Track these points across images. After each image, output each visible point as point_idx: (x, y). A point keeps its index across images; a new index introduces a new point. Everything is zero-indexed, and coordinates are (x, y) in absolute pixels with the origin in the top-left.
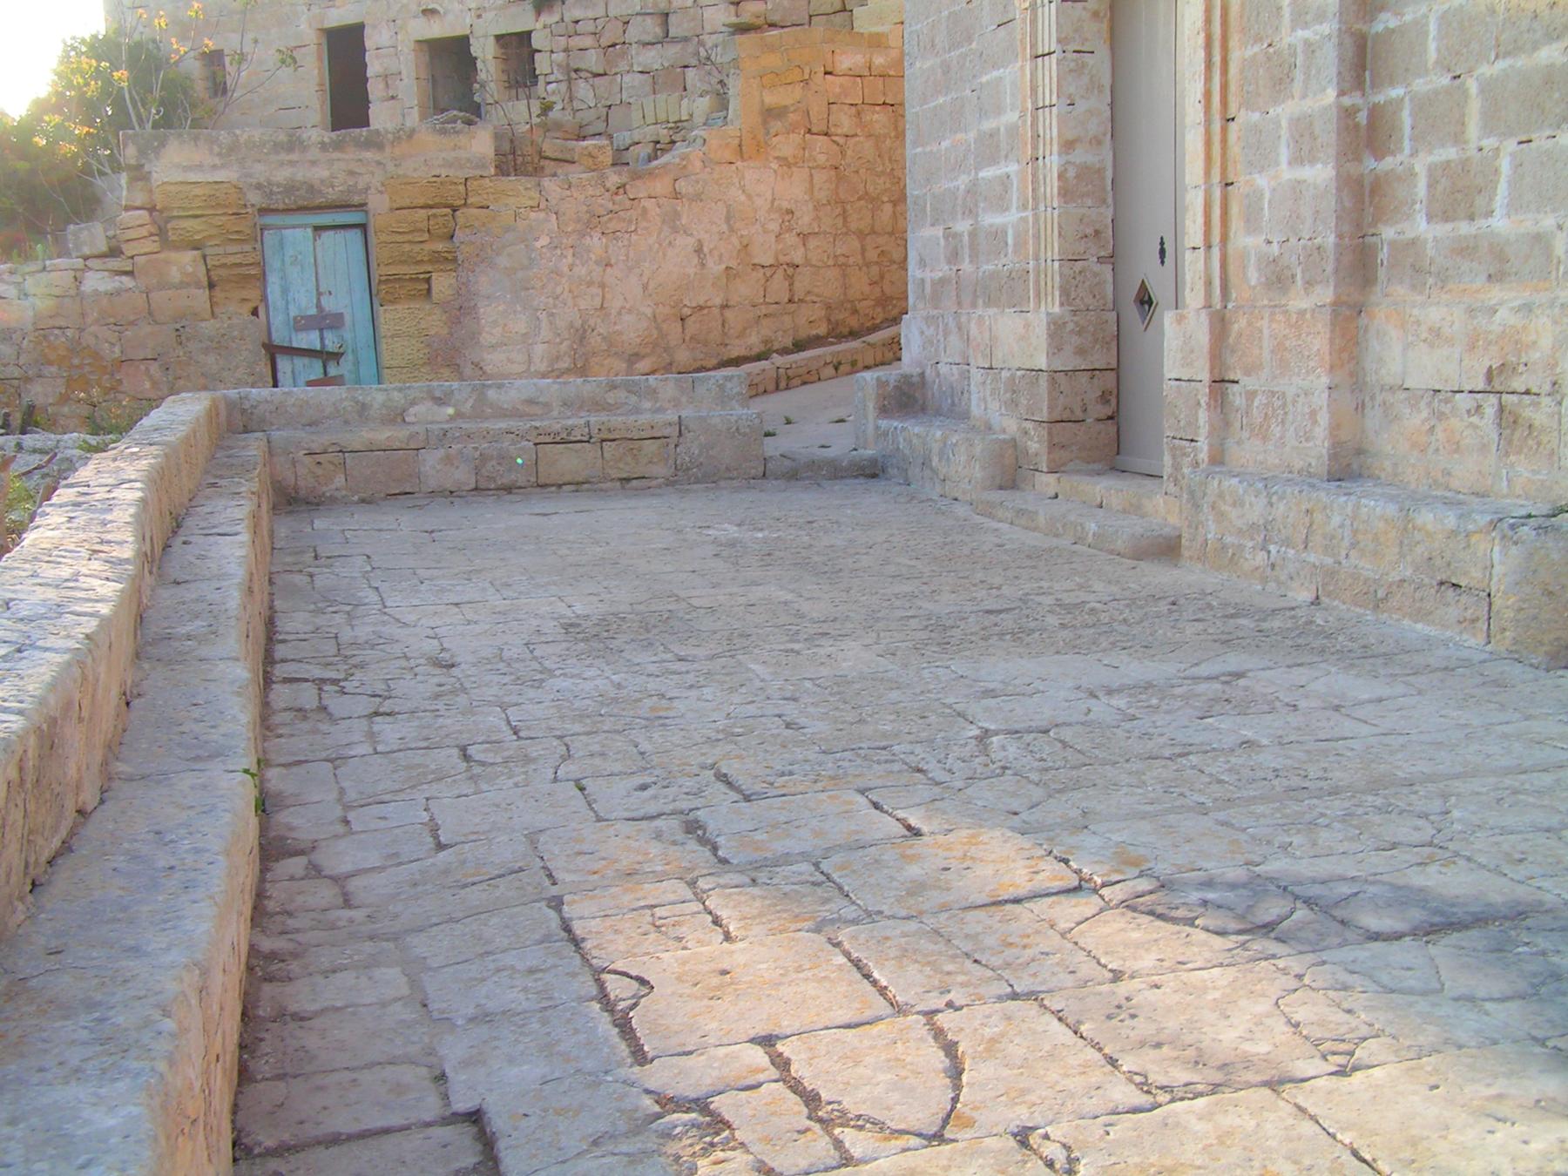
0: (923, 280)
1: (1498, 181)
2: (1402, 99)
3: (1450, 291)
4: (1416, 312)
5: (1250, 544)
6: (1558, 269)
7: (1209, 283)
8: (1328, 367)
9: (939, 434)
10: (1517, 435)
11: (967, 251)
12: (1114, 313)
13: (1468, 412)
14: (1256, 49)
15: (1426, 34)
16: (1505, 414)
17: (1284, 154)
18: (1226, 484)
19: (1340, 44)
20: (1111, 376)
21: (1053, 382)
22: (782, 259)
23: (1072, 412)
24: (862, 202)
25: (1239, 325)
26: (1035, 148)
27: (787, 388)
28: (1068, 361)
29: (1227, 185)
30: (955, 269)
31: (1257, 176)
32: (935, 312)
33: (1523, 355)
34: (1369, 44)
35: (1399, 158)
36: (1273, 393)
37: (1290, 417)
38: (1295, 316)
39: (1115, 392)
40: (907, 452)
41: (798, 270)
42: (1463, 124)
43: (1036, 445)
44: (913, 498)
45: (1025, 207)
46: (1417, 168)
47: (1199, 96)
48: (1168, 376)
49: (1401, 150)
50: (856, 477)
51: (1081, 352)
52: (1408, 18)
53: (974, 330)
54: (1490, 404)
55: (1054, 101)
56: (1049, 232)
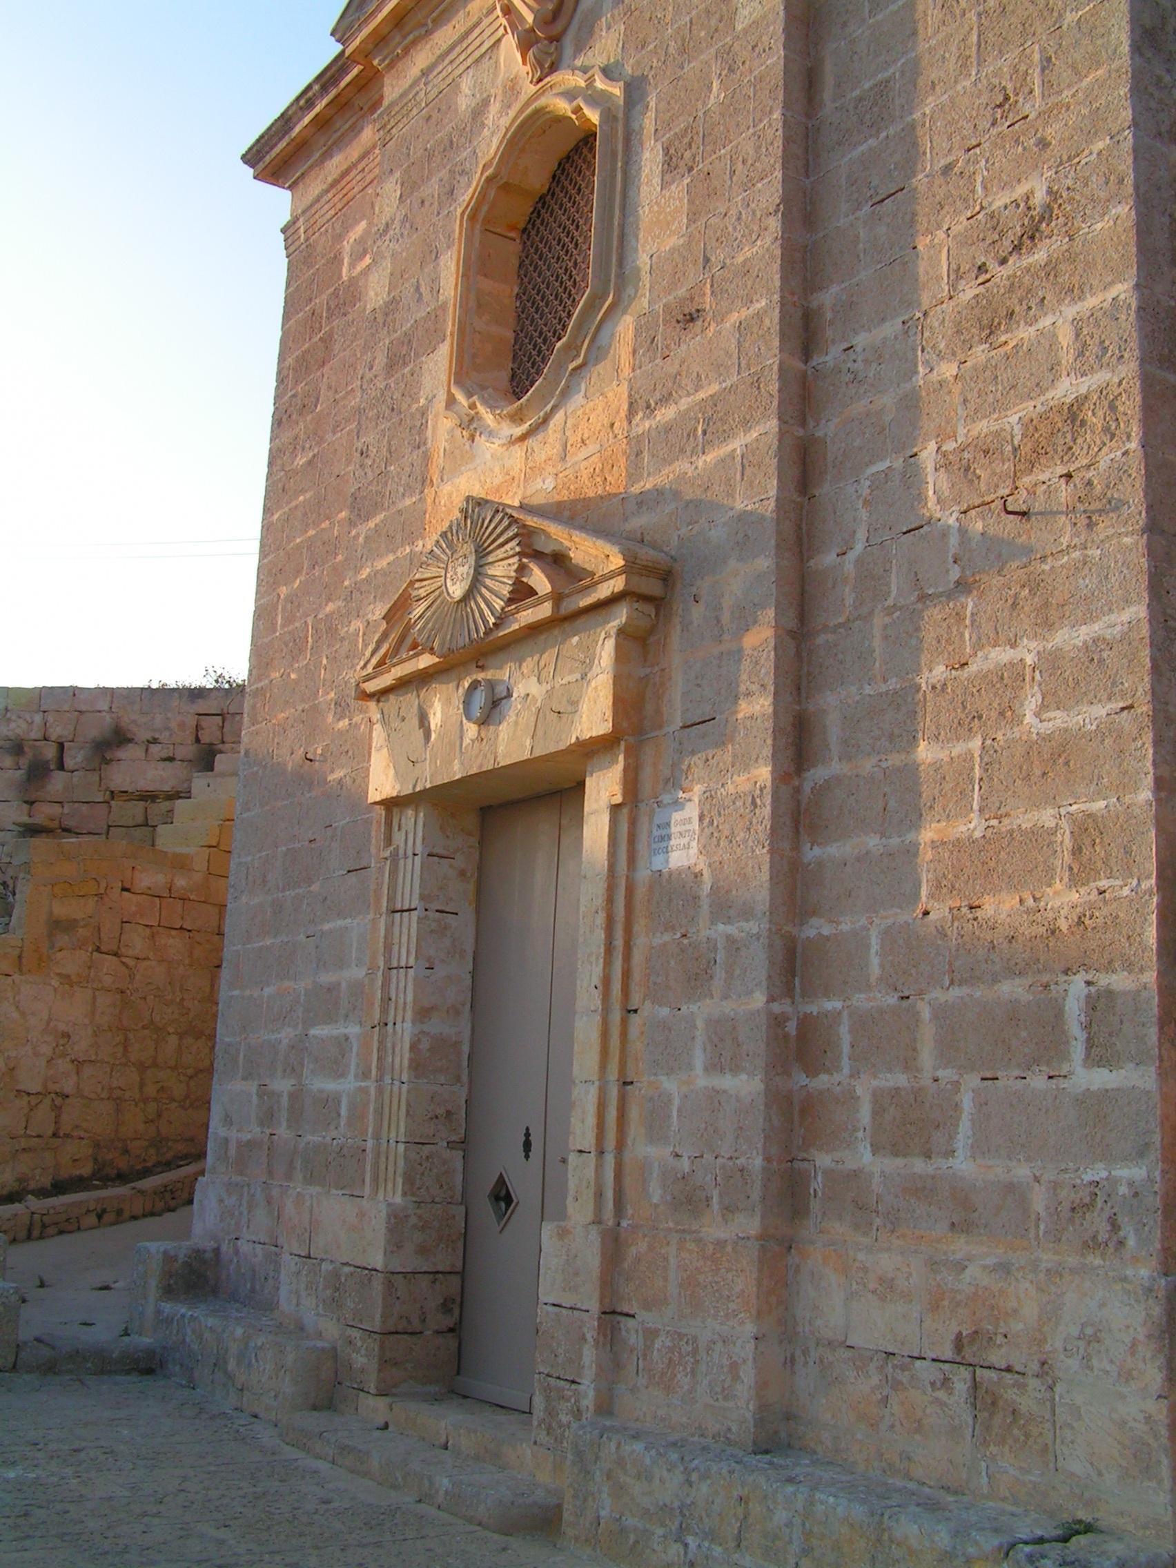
0: (227, 1140)
1: (959, 1118)
2: (840, 1013)
3: (904, 1236)
4: (861, 1256)
5: (660, 1531)
6: (1037, 1227)
7: (599, 1195)
8: (754, 1312)
9: (239, 1331)
10: (997, 1420)
11: (285, 1114)
12: (463, 1207)
13: (933, 1384)
14: (667, 937)
15: (868, 947)
16: (981, 1393)
17: (699, 1059)
18: (627, 1448)
19: (771, 946)
20: (455, 1280)
21: (389, 1286)
22: (51, 1087)
23: (409, 1322)
24: (146, 1032)
25: (638, 1248)
26: (385, 1011)
27: (41, 1237)
28: (408, 1261)
29: (625, 1083)
30: (268, 1131)
31: (663, 1078)
32: (237, 1179)
33: (1002, 1324)
34: (799, 949)
35: (837, 1077)
36: (681, 1336)
37: (703, 1368)
38: (711, 1247)
39: (458, 1300)
40: (195, 1347)
41: (68, 1101)
42: (914, 1050)
43: (363, 1359)
44: (201, 1411)
45: (366, 1075)
46: (859, 1091)
47: (596, 980)
48: (543, 1299)
49: (839, 1069)
50: (128, 1372)
51: (423, 1250)
52: (845, 927)
53: (290, 1208)
54: (961, 1380)
55: (412, 962)
56: (395, 1107)
